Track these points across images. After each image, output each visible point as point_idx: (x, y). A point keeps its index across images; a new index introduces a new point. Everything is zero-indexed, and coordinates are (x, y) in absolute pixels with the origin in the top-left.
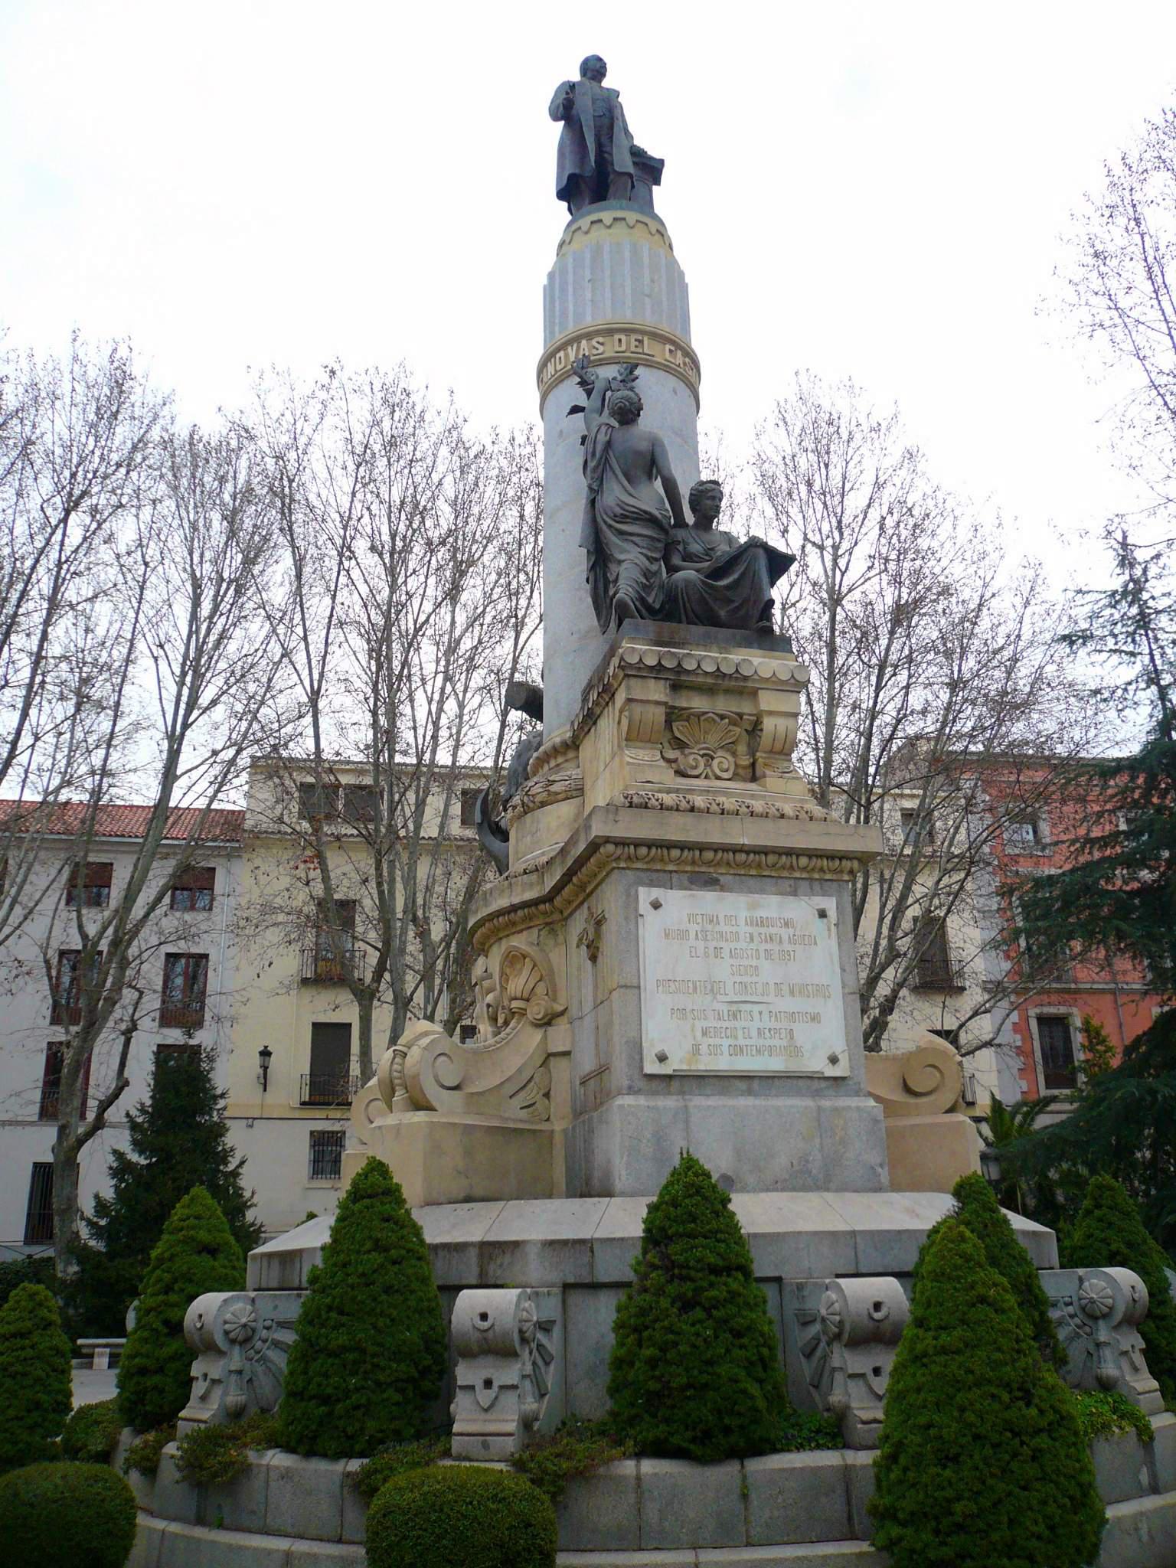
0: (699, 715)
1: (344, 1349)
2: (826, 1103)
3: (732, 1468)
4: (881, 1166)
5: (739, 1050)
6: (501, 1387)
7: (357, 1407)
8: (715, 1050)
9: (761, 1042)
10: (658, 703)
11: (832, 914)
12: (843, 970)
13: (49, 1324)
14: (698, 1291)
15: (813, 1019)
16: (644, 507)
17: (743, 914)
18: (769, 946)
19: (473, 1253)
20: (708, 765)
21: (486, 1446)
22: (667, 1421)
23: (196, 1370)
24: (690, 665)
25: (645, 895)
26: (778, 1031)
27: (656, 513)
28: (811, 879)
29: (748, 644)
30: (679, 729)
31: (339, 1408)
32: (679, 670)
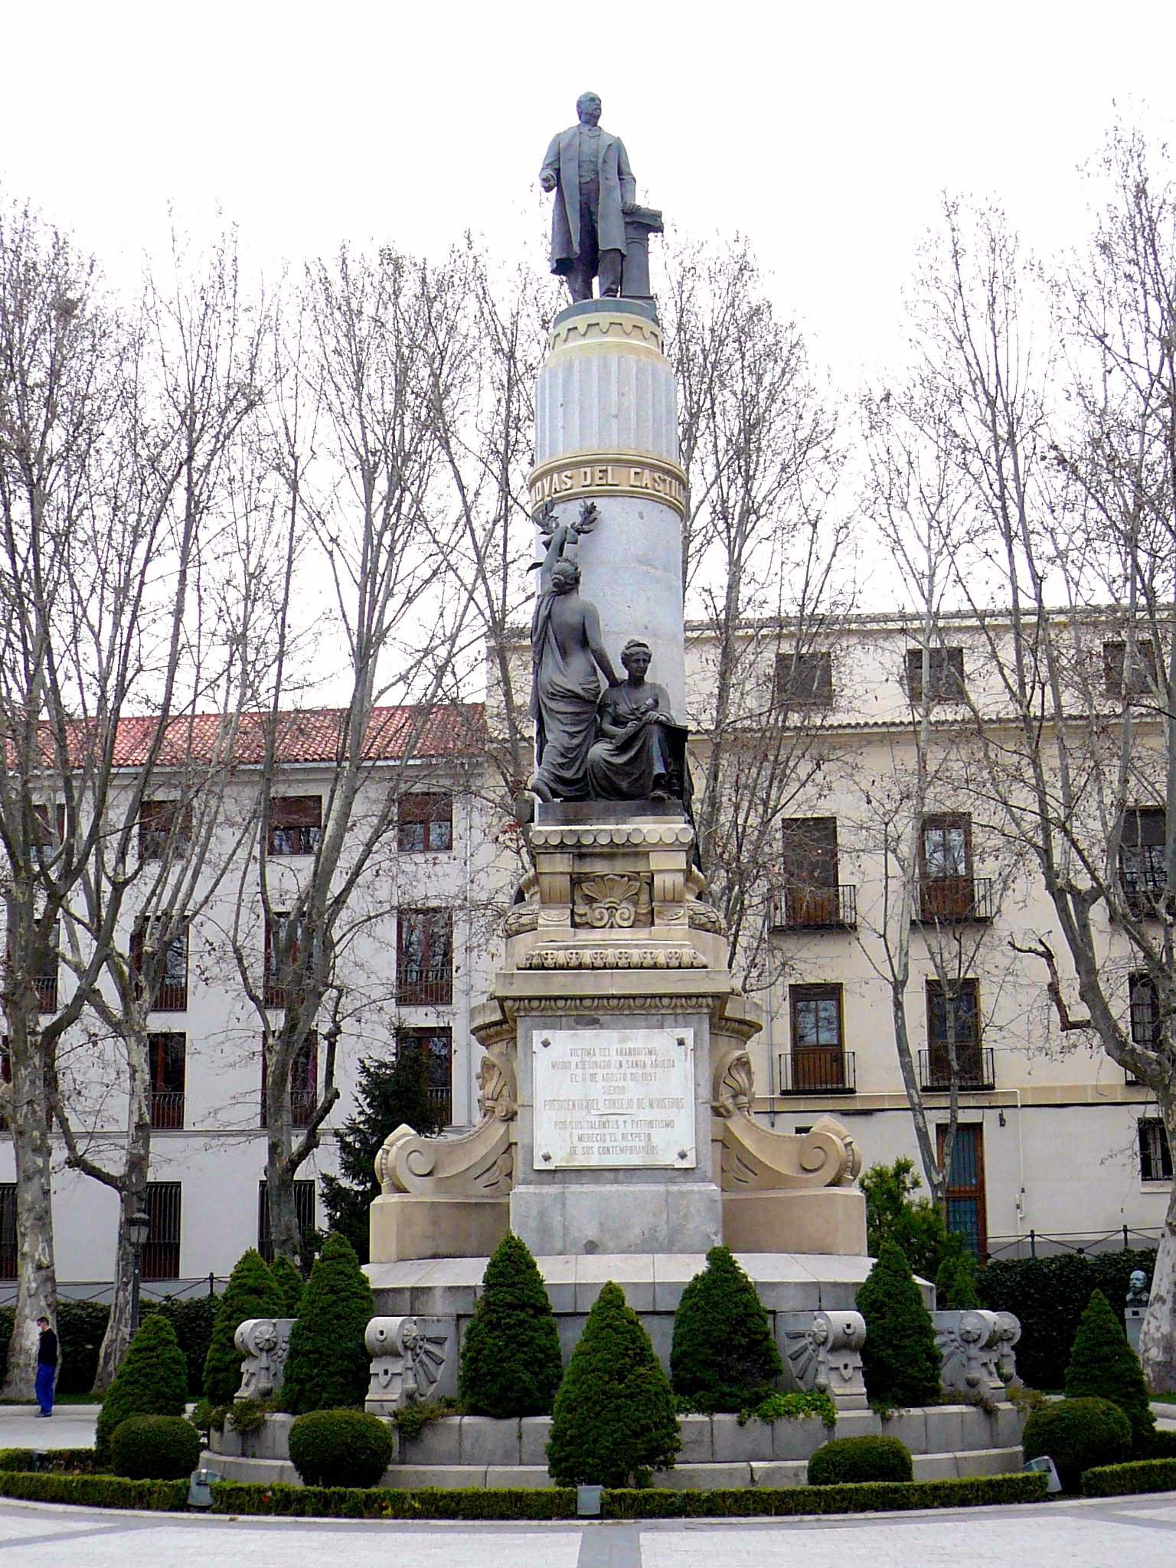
0: (602, 877)
1: (310, 1352)
2: (674, 1188)
3: (515, 1421)
4: (716, 1234)
5: (607, 1151)
6: (394, 1374)
7: (317, 1385)
8: (588, 1151)
9: (624, 1144)
10: (562, 873)
11: (690, 1042)
12: (697, 1085)
13: (169, 1342)
14: (499, 1319)
15: (667, 1125)
16: (569, 687)
17: (615, 1046)
18: (634, 1071)
19: (408, 1294)
20: (611, 916)
21: (382, 1407)
22: (478, 1394)
23: (244, 1367)
24: (587, 841)
25: (538, 1036)
26: (638, 1135)
27: (579, 690)
28: (675, 1014)
29: (641, 812)
30: (587, 888)
31: (308, 1386)
32: (579, 845)
